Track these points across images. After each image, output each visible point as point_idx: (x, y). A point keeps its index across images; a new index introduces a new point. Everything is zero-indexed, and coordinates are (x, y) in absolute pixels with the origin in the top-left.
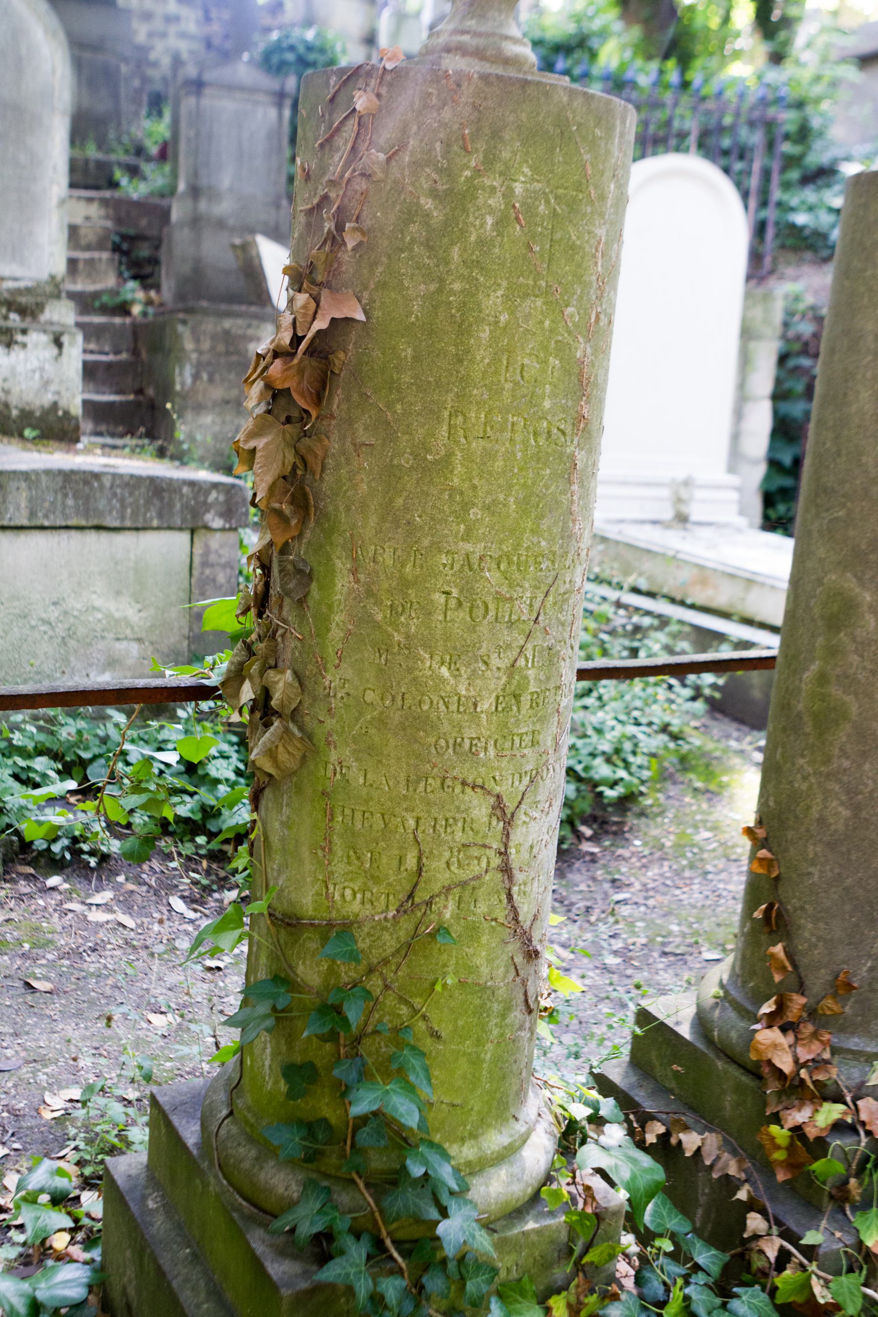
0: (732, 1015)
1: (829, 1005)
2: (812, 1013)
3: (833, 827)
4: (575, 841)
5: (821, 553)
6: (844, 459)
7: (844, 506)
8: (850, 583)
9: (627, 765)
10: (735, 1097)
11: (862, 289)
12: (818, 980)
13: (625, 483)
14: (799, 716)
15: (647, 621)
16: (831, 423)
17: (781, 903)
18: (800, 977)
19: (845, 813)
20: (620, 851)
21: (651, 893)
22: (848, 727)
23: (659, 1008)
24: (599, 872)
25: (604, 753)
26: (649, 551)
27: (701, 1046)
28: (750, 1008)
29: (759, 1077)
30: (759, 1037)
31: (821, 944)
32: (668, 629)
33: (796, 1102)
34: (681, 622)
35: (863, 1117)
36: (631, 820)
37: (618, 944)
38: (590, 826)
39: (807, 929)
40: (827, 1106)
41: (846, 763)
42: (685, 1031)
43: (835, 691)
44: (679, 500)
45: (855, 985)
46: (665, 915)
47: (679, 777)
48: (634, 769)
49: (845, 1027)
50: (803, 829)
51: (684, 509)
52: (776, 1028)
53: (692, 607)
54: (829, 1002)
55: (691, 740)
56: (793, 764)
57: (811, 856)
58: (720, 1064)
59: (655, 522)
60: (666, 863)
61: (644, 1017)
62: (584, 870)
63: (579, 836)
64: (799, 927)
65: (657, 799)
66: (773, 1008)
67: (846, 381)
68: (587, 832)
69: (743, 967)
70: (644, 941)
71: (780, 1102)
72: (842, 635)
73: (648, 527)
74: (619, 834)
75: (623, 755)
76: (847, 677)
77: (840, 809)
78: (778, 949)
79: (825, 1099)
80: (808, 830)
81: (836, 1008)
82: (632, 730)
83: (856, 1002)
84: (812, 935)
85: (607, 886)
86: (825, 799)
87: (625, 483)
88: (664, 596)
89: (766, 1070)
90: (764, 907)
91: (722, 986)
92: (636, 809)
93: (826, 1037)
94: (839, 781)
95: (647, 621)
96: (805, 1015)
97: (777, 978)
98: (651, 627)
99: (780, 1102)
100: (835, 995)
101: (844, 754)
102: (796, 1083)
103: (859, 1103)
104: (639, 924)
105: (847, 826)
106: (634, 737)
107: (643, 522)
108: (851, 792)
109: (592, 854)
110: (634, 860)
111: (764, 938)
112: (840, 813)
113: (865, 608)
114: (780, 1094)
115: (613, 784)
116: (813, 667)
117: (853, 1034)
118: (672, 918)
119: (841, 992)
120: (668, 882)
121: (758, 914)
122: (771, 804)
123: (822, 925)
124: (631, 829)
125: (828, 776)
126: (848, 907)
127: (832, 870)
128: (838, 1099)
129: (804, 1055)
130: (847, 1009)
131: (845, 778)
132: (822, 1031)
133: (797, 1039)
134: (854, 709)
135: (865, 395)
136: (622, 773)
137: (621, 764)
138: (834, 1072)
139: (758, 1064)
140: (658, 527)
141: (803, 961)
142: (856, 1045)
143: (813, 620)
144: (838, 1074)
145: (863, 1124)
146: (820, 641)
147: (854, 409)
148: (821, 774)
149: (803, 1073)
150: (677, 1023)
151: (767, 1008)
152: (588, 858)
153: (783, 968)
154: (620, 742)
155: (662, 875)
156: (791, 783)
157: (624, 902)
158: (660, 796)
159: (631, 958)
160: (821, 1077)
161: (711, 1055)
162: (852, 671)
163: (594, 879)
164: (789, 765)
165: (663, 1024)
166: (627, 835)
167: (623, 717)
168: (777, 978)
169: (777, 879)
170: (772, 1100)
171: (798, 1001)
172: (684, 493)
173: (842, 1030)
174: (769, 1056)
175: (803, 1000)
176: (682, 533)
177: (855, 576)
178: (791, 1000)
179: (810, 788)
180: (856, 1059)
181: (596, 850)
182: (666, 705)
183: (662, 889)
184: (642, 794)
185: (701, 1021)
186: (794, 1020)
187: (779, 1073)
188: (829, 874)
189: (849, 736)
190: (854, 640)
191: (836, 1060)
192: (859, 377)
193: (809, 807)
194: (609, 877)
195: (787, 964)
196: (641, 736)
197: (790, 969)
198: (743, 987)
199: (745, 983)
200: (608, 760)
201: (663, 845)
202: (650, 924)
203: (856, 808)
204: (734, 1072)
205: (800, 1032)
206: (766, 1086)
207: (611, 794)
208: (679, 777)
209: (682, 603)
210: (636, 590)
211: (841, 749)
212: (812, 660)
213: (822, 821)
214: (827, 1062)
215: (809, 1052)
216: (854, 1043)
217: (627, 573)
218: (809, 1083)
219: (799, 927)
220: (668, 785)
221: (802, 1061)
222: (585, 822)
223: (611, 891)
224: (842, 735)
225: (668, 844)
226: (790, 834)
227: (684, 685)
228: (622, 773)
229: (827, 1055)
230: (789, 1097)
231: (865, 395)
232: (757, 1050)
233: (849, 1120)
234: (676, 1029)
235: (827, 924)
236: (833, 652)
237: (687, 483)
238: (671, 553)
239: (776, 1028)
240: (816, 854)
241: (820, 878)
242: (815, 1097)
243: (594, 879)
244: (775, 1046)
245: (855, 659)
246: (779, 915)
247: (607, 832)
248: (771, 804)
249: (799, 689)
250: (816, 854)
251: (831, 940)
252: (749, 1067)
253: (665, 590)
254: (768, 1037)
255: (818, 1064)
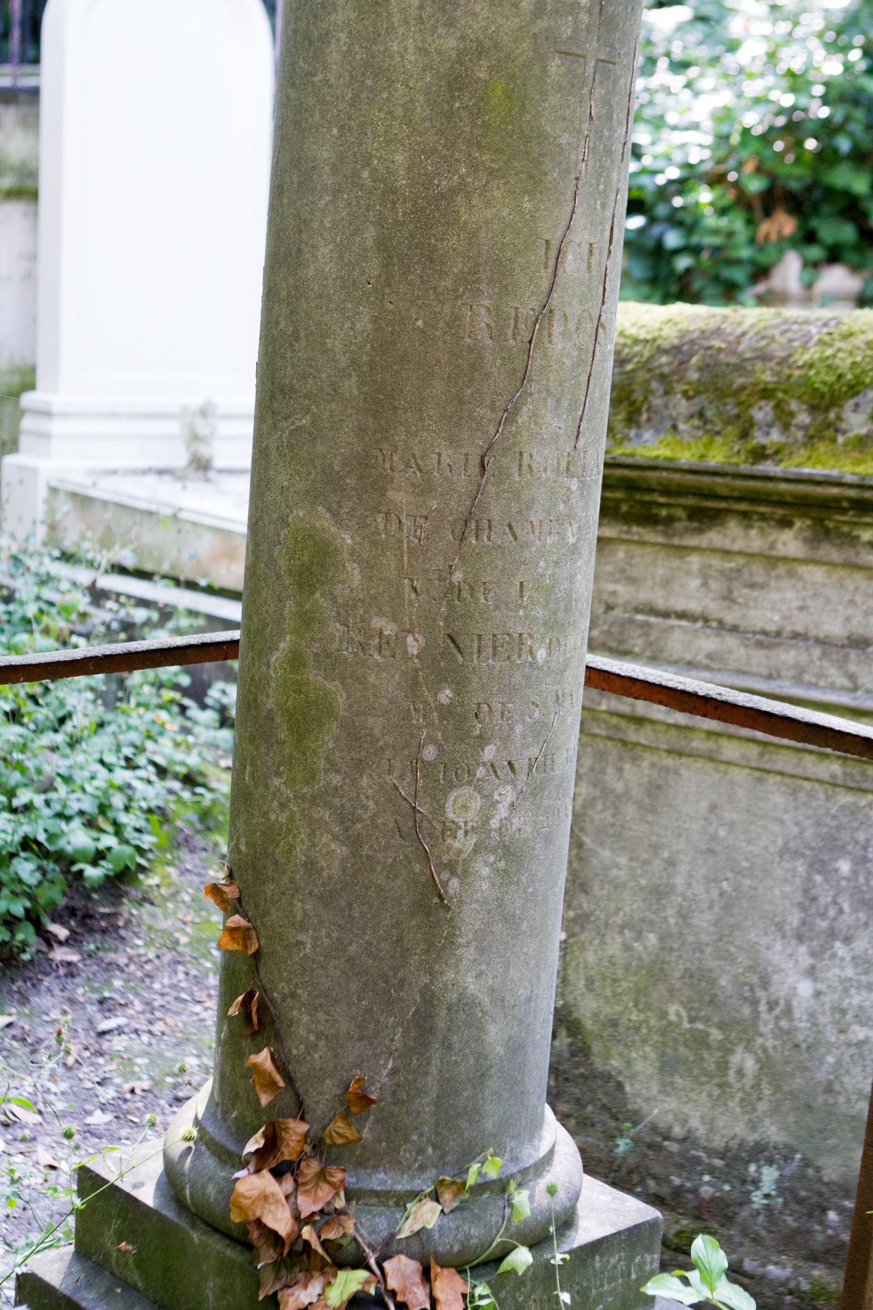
0: (209, 1161)
1: (340, 1128)
2: (318, 1145)
3: (325, 874)
4: (44, 948)
5: (283, 479)
6: (303, 343)
7: (308, 411)
8: (323, 521)
9: (118, 829)
10: (219, 1281)
11: (312, 101)
12: (322, 1097)
13: (114, 416)
14: (270, 717)
15: (140, 615)
16: (283, 293)
17: (264, 990)
18: (297, 1095)
19: (341, 850)
20: (111, 956)
21: (158, 1014)
22: (335, 727)
23: (107, 1168)
24: (80, 991)
25: (81, 813)
26: (150, 514)
27: (170, 1213)
28: (233, 1148)
29: (249, 1246)
30: (240, 1187)
31: (322, 1043)
32: (171, 625)
33: (301, 1276)
34: (192, 613)
35: (392, 1284)
36: (127, 908)
37: (108, 1094)
38: (64, 924)
39: (302, 1024)
40: (342, 1275)
41: (337, 779)
42: (147, 1196)
43: (314, 676)
44: (195, 438)
45: (373, 1097)
46: (178, 1045)
47: (199, 841)
48: (129, 833)
49: (366, 1160)
50: (285, 880)
51: (204, 451)
52: (265, 1173)
53: (210, 590)
54: (339, 1126)
55: (214, 785)
56: (267, 787)
57: (299, 917)
58: (195, 1236)
59: (161, 472)
60: (180, 968)
61: (87, 1179)
62: (57, 991)
63: (49, 940)
64: (292, 1023)
65: (169, 876)
66: (261, 1143)
67: (300, 231)
68: (62, 932)
69: (222, 1091)
70: (146, 1085)
71: (277, 1278)
72: (317, 595)
73: (152, 479)
74: (111, 930)
75: (111, 814)
76: (328, 655)
77: (333, 846)
78: (263, 1058)
79: (341, 1265)
80: (292, 881)
81: (350, 1134)
82: (122, 776)
83: (377, 1121)
84: (309, 1031)
85: (92, 1009)
86: (312, 835)
87: (114, 416)
88: (164, 577)
89: (255, 1235)
90: (240, 998)
91: (197, 1122)
92: (135, 893)
93: (338, 1176)
94: (329, 805)
95: (140, 615)
96: (307, 1149)
97: (265, 1099)
98: (147, 623)
99: (277, 1278)
100: (346, 1116)
101: (332, 766)
102: (299, 1247)
103: (387, 1265)
104: (139, 1061)
105: (344, 869)
106: (129, 786)
107: (145, 472)
108: (346, 819)
109: (69, 964)
110: (132, 967)
111: (245, 1044)
112: (333, 851)
113: (346, 555)
114: (278, 1265)
115: (99, 857)
116: (282, 645)
117: (376, 1167)
118: (190, 1048)
119: (354, 1109)
120: (184, 996)
121: (233, 1011)
122: (243, 848)
123: (321, 1016)
124: (128, 922)
125: (314, 800)
126: (354, 987)
127: (329, 935)
128: (359, 1263)
129: (307, 1205)
130: (366, 1133)
131: (337, 801)
132: (332, 1169)
133: (297, 1184)
134: (341, 701)
135: (325, 251)
136: (109, 841)
137: (110, 828)
138: (350, 1226)
139: (244, 1227)
140: (166, 478)
141: (299, 1071)
142: (382, 1182)
143: (279, 577)
144: (359, 1227)
145: (393, 1294)
146: (290, 606)
147: (311, 272)
148: (303, 797)
149: (307, 1232)
150: (136, 1186)
151: (254, 1144)
152: (62, 971)
153: (272, 1084)
154: (105, 793)
155: (174, 987)
156: (265, 814)
157: (120, 1031)
158: (171, 870)
159: (128, 1112)
160: (332, 1235)
161: (183, 1223)
162: (335, 645)
163: (72, 1001)
164: (261, 789)
165: (114, 1189)
166: (122, 932)
167: (109, 758)
168: (265, 1099)
169: (257, 955)
170: (268, 1277)
171: (296, 1130)
172: (202, 428)
173: (360, 1164)
174: (258, 1213)
175: (303, 1128)
176: (204, 487)
177: (329, 510)
178: (286, 1129)
179: (291, 819)
180: (384, 1204)
181: (75, 958)
182: (180, 738)
183: (175, 1006)
184: (141, 869)
185: (172, 1179)
186: (294, 1157)
187: (274, 1237)
188: (326, 941)
189: (337, 739)
190: (334, 599)
191: (353, 1207)
192: (315, 225)
193: (292, 847)
194: (96, 996)
195: (278, 1078)
196: (136, 784)
197: (281, 1084)
198: (224, 1119)
199: (225, 1113)
200: (90, 824)
201: (177, 942)
202: (155, 1059)
203: (355, 843)
204: (217, 1244)
205: (301, 1174)
206: (256, 1258)
207: (93, 873)
208: (199, 841)
209: (191, 585)
210: (122, 570)
211: (327, 759)
212: (281, 635)
213: (310, 866)
214: (339, 1212)
215: (315, 1202)
216: (379, 1180)
217: (106, 543)
218: (316, 1245)
219: (292, 1023)
220: (184, 854)
221: (304, 1215)
222: (57, 918)
223: (99, 1016)
224: (328, 740)
225: (184, 940)
226: (270, 889)
227: (204, 707)
228: (109, 841)
229: (340, 1203)
230: (290, 1270)
231: (325, 251)
232: (240, 1208)
233: (372, 1291)
234: (135, 1193)
235: (328, 1013)
236: (308, 620)
237: (204, 412)
238: (167, 511)
239: (265, 1173)
240: (305, 914)
241: (314, 947)
242: (324, 1264)
243: (72, 1001)
244: (265, 1198)
245: (335, 628)
246: (263, 1008)
247: (91, 930)
248: (243, 848)
249: (267, 678)
250: (305, 914)
251: (336, 1036)
252: (235, 1234)
253: (165, 568)
254: (253, 1184)
255: (327, 1216)
